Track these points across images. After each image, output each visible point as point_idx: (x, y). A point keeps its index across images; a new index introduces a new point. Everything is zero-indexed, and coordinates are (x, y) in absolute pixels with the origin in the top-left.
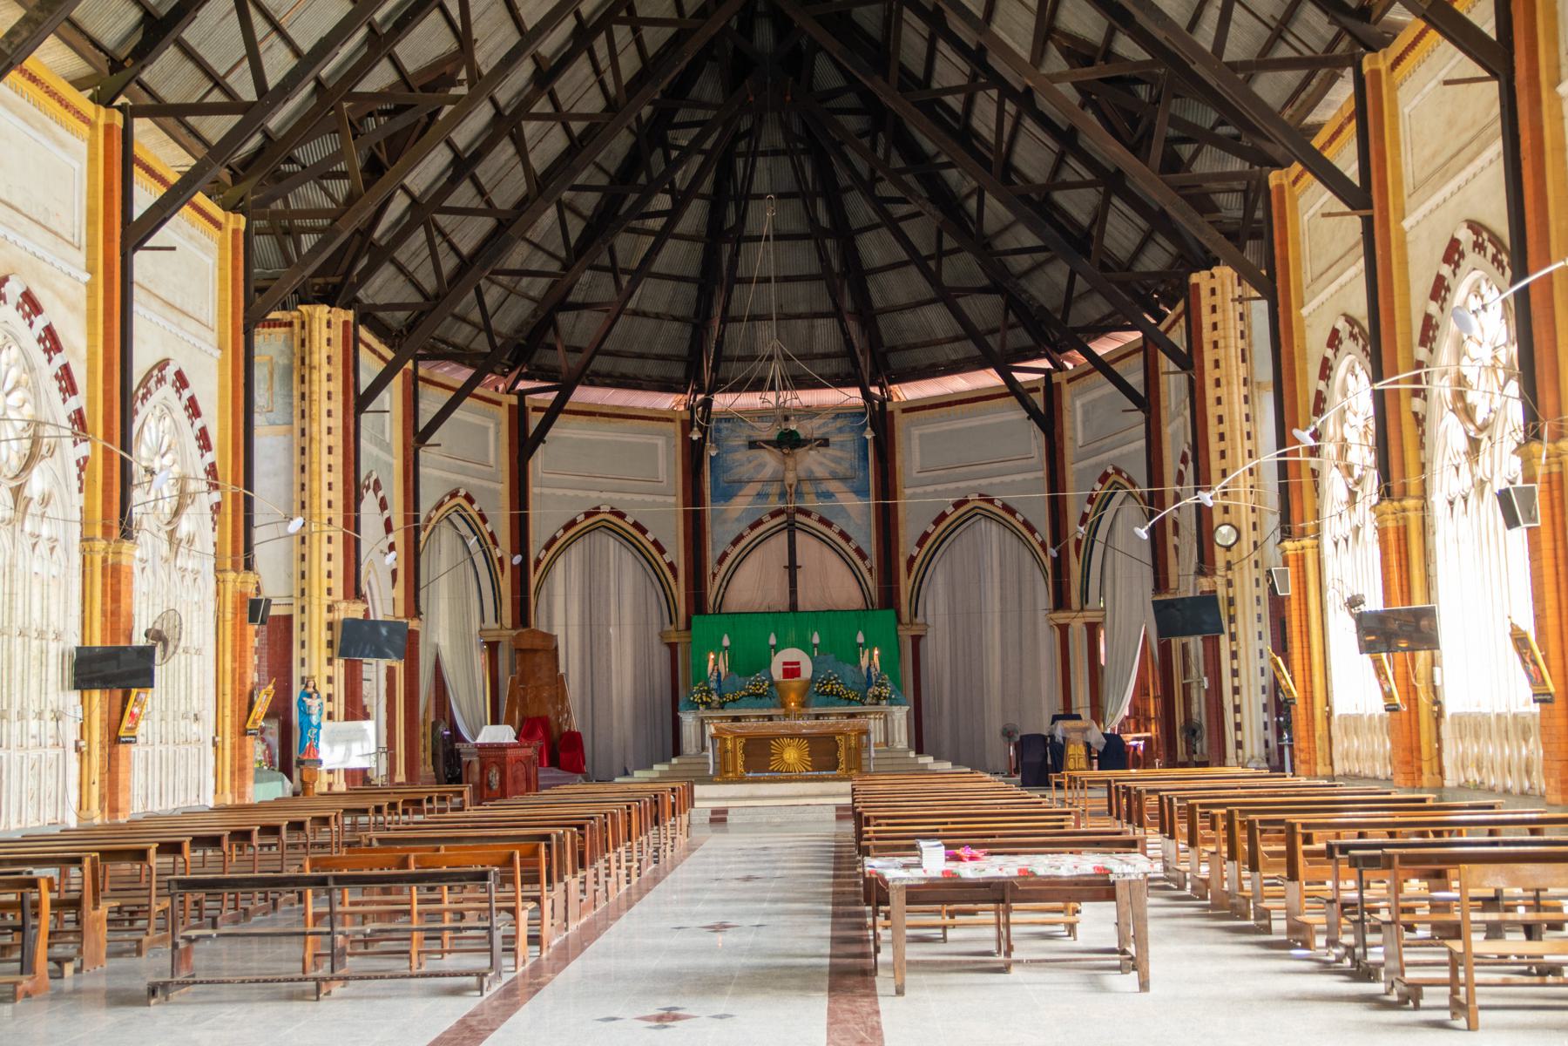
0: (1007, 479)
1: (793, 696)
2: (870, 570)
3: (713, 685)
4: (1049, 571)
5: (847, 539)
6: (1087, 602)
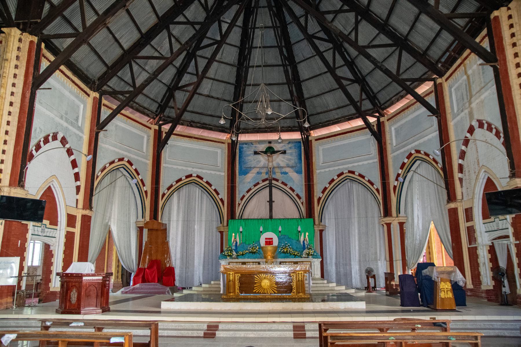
0: (360, 163)
1: (269, 253)
2: (302, 203)
3: (234, 248)
4: (381, 201)
5: (293, 190)
6: (399, 213)
